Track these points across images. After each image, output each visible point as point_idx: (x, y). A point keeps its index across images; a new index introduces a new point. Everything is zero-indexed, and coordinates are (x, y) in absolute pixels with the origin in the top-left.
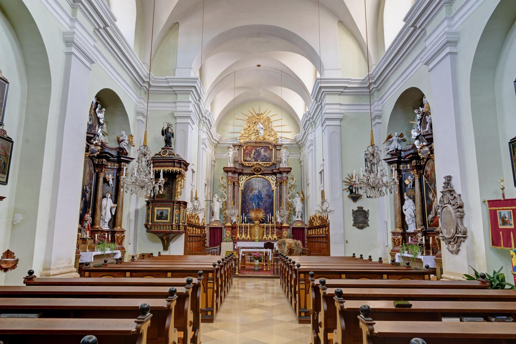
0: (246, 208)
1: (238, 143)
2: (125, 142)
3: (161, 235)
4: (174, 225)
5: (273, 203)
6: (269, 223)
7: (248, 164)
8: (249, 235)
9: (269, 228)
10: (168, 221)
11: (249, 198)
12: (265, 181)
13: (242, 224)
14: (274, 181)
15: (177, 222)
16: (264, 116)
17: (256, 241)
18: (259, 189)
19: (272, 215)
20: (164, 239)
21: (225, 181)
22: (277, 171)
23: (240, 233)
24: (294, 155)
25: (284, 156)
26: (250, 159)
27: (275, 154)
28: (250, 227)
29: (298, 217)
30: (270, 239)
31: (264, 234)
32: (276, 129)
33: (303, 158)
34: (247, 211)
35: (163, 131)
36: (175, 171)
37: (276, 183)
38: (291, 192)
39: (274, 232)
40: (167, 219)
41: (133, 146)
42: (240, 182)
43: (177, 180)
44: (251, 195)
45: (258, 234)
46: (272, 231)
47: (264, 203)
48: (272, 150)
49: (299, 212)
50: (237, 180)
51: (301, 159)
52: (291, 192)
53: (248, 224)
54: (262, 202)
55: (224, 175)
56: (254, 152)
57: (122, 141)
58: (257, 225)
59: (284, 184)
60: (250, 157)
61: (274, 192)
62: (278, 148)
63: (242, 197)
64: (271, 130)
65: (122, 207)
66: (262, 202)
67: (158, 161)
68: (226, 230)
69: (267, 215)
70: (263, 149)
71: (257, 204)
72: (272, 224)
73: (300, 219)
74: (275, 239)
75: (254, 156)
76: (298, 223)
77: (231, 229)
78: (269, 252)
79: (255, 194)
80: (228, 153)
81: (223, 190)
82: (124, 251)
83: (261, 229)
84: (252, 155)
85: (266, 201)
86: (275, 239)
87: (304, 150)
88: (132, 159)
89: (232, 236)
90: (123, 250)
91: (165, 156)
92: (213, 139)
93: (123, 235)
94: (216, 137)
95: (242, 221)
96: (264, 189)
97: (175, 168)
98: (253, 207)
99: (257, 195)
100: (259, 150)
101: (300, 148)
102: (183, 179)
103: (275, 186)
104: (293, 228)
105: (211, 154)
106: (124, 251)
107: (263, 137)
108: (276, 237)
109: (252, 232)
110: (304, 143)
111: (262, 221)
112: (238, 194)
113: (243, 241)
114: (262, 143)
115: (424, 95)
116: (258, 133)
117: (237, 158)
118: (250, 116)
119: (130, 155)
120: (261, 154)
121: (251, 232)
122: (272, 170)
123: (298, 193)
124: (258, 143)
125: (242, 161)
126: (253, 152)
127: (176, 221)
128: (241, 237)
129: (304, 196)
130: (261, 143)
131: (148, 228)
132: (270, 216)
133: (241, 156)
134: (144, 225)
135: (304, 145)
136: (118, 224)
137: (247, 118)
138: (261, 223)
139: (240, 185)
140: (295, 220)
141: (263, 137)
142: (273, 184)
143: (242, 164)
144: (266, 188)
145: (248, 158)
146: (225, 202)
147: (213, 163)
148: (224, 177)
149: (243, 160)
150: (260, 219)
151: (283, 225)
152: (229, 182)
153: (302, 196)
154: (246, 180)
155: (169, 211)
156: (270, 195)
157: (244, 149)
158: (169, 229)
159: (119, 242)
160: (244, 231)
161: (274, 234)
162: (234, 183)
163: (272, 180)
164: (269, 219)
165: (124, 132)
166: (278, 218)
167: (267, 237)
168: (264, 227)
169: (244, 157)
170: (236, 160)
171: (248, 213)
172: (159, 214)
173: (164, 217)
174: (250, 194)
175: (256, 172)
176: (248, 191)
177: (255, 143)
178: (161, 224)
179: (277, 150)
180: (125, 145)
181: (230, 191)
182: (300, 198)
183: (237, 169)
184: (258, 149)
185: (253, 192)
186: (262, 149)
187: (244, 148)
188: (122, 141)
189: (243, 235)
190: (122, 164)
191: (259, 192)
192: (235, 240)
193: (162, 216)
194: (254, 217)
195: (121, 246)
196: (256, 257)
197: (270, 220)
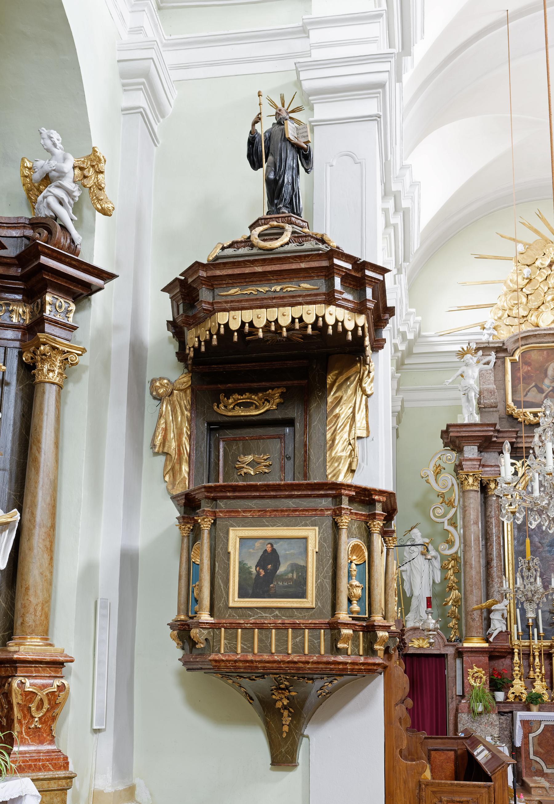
1: (491, 339)
2: (60, 187)
3: (265, 684)
4: (346, 625)
7: (535, 415)
10: (310, 601)
15: (356, 607)
20: (279, 705)
35: (252, 142)
36: (335, 326)
40: (303, 595)
41: (105, 212)
43: (330, 399)
57: (47, 180)
65: (53, 527)
67: (237, 271)
77: (485, 659)
80: (459, 372)
81: (444, 516)
82: (61, 773)
84: (547, 382)
88: (107, 276)
90: (57, 767)
91: (276, 244)
93: (57, 682)
97: (332, 308)
102: (364, 391)
106: (61, 773)
119: (92, 256)
127: (350, 601)
131: (193, 644)
134: (172, 626)
136: (30, 619)
137: (520, 248)
143: (511, 416)
146: (455, 558)
148: (443, 465)
155: (313, 546)
157: (513, 363)
158: (314, 649)
159: (36, 723)
165: (56, 136)
172: (252, 564)
173: (281, 578)
178: (268, 618)
180: (61, 203)
188: (47, 180)
190: (48, 298)
193: (271, 575)
195: (46, 747)
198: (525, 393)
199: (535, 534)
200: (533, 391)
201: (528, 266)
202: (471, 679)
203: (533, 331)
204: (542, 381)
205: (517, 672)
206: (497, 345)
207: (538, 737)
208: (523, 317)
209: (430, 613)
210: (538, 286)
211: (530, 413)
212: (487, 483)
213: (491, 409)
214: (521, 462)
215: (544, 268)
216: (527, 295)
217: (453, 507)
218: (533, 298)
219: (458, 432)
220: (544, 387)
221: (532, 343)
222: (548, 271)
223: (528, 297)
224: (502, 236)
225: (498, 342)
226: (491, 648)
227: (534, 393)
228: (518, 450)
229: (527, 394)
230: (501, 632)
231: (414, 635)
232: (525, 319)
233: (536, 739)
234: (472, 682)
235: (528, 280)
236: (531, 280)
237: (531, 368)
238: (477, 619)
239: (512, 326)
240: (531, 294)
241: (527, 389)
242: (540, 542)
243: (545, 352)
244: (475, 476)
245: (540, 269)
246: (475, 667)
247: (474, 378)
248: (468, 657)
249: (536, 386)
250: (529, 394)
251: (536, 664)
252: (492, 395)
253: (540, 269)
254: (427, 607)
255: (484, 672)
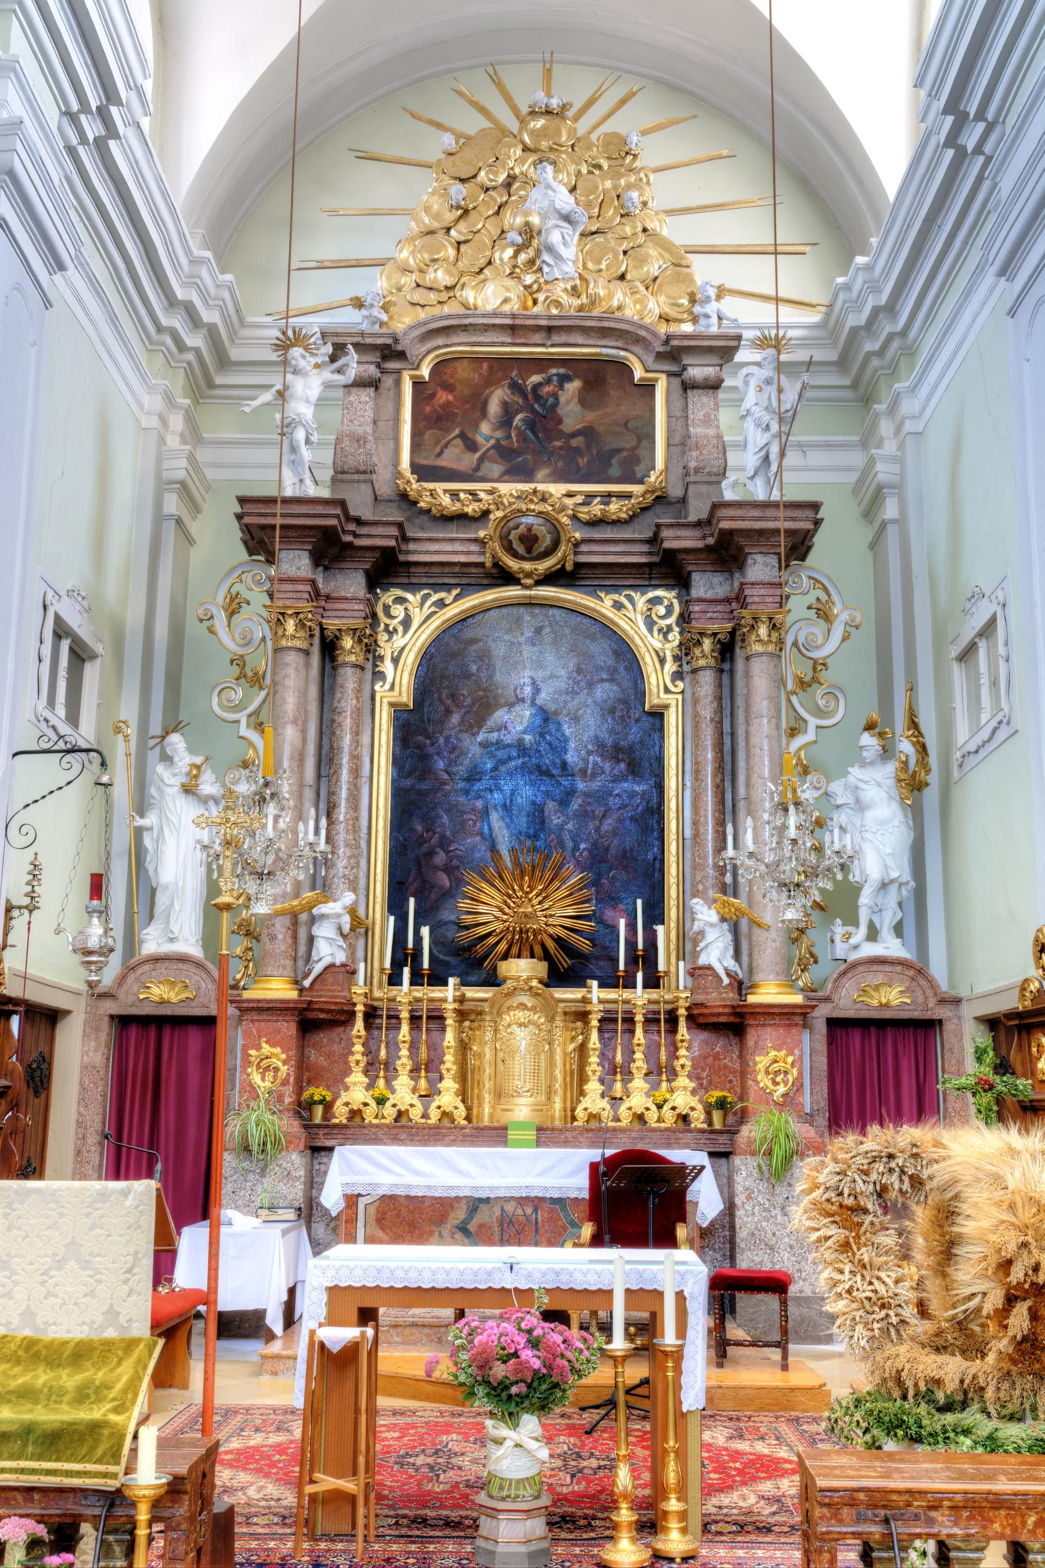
0: (430, 854)
5: (657, 811)
6: (630, 984)
7: (454, 495)
8: (449, 1085)
9: (629, 1020)
11: (461, 770)
12: (592, 637)
13: (394, 991)
14: (665, 632)
16: (582, 126)
17: (512, 1135)
18: (543, 697)
19: (655, 914)
21: (260, 630)
22: (700, 544)
23: (371, 1068)
24: (816, 458)
25: (758, 412)
26: (469, 460)
27: (679, 419)
28: (462, 1015)
29: (873, 935)
30: (640, 1118)
31: (583, 1079)
32: (670, 229)
33: (900, 460)
34: (444, 880)
37: (686, 649)
38: (813, 722)
39: (673, 1055)
42: (382, 637)
44: (472, 746)
45: (536, 1073)
46: (652, 1052)
47: (584, 815)
48: (648, 389)
49: (884, 886)
50: (357, 623)
51: (879, 466)
52: (813, 722)
53: (449, 992)
54: (564, 803)
55: (248, 578)
56: (505, 405)
58: (526, 999)
59: (758, 648)
60: (471, 446)
61: (672, 719)
62: (697, 372)
63: (397, 762)
64: (641, 238)
66: (564, 803)
68: (247, 1034)
69: (609, 914)
70: (574, 386)
71: (523, 821)
72: (654, 994)
73: (890, 947)
74: (685, 1118)
75: (499, 434)
76: (879, 979)
77: (288, 1028)
78: (680, 1297)
79: (508, 739)
83: (558, 1032)
84: (485, 428)
85: (602, 796)
86: (685, 1118)
87: (914, 389)
89: (299, 1090)
92: (171, 301)
94: (192, 281)
95: (397, 964)
96: (583, 697)
98: (493, 849)
99: (520, 746)
100: (547, 389)
101: (867, 400)
103: (678, 676)
104: (832, 1023)
105: (155, 422)
107: (575, 292)
108: (694, 1102)
109: (480, 1056)
110: (913, 333)
111: (565, 962)
112: (366, 740)
113: (396, 1140)
114: (563, 338)
115: (159, 1439)
116: (538, 253)
117: (359, 440)
118: (472, 131)
120: (560, 421)
121: (472, 1061)
122: (654, 540)
123: (870, 727)
124: (538, 338)
125: (398, 475)
126: (494, 407)
128: (381, 1101)
129: (923, 749)
130: (556, 338)
132: (632, 927)
133: (397, 440)
135: (910, 352)
137: (448, 141)
138: (557, 977)
139: (387, 667)
140: (853, 957)
141: (575, 292)
142: (662, 661)
143: (404, 496)
144: (603, 691)
145: (455, 457)
147: (172, 504)
149: (415, 468)
150: (551, 945)
151: (752, 999)
152: (290, 625)
153: (906, 747)
154: (436, 623)
156: (631, 749)
157: (418, 384)
160: (414, 1046)
161: (673, 1074)
162: (329, 648)
163: (650, 624)
164: (631, 944)
166: (711, 935)
167: (615, 1100)
168: (583, 1016)
169: (416, 445)
170: (357, 458)
171: (448, 894)
174: (467, 740)
175: (515, 555)
176: (448, 712)
177: (513, 329)
179: (688, 386)
181: (290, 703)
182: (890, 769)
183: (359, 521)
184: (536, 379)
185: (490, 723)
186: (564, 379)
187: (425, 372)
189: (403, 1082)
191: (546, 718)
192: (328, 1127)
194: (498, 926)
196: (499, 1371)
197: (633, 959)
198: (438, 450)
199: (438, 754)
200: (456, 446)
201: (462, 181)
202: (255, 1073)
203: (459, 316)
204: (476, 426)
205: (358, 1057)
206: (380, 341)
207: (377, 1204)
208: (447, 288)
209: (94, 911)
210: (480, 226)
211: (445, 491)
212: (336, 637)
213: (356, 477)
214: (418, 597)
215: (494, 188)
216: (459, 243)
217: (261, 688)
218: (469, 251)
219: (261, 515)
220: (479, 439)
221: (459, 344)
222: (501, 196)
223: (458, 250)
224: (414, 116)
225: (381, 335)
226: (301, 1002)
227: (457, 451)
228: (412, 570)
229: (441, 452)
230: (332, 966)
231: (154, 974)
232: (451, 294)
233: (372, 1210)
234: (256, 1078)
235: (460, 212)
236: (466, 212)
237: (455, 397)
238: (280, 937)
239: (423, 306)
240: (466, 242)
241: (444, 442)
242: (446, 771)
243: (485, 365)
244: (301, 616)
245: (487, 189)
246: (264, 1045)
247: (308, 401)
248: (253, 1021)
249: (462, 436)
250: (447, 451)
251: (591, 1045)
252: (360, 446)
253: (487, 189)
254: (92, 898)
255: (284, 1056)
